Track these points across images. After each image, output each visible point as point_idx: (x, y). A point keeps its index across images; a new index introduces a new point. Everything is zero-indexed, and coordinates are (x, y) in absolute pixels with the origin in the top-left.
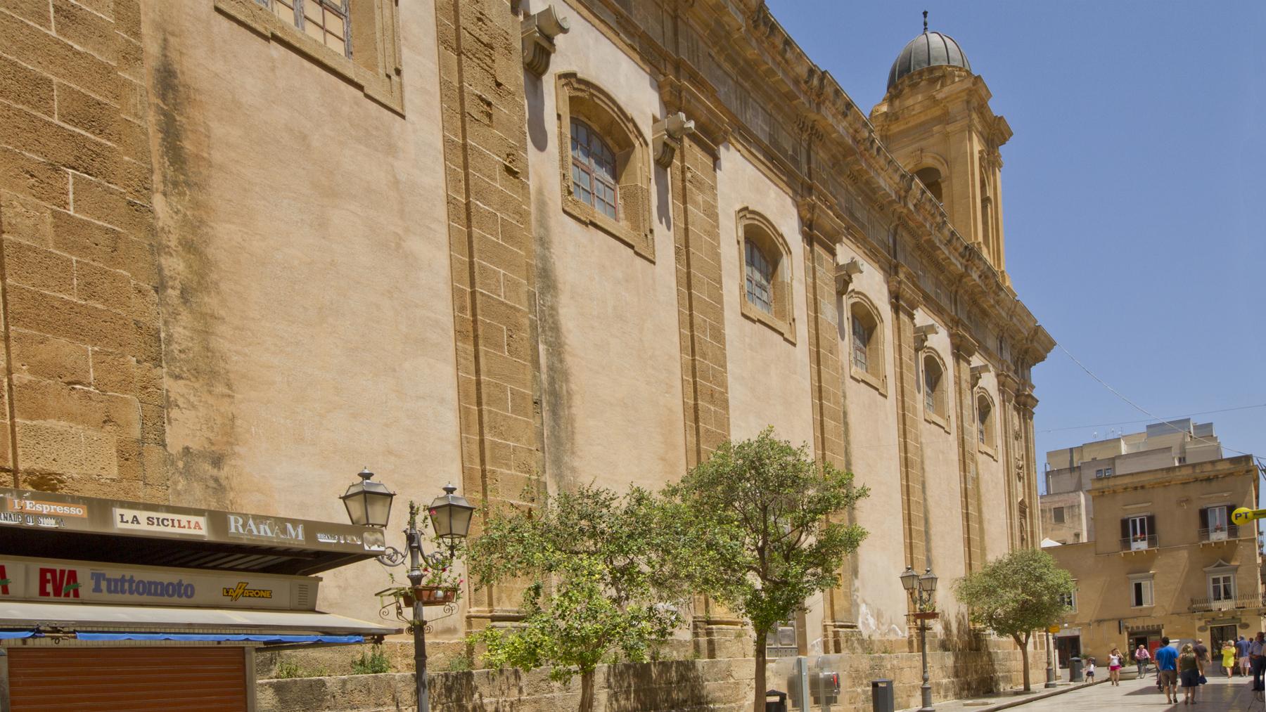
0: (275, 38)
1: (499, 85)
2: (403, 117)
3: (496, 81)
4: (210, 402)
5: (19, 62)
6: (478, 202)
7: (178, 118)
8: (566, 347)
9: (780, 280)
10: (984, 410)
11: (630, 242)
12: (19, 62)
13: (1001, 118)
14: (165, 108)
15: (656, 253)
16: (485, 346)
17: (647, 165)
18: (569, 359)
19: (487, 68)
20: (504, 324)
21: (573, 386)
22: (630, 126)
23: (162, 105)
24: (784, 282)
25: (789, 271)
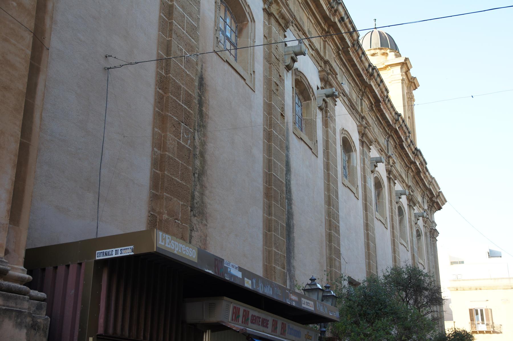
0: (227, 62)
1: (280, 76)
2: (254, 92)
3: (280, 75)
4: (201, 228)
5: (176, 80)
6: (274, 131)
7: (203, 98)
8: (293, 201)
9: (352, 165)
10: (419, 235)
11: (311, 147)
12: (176, 80)
13: (415, 77)
14: (200, 94)
15: (318, 152)
16: (274, 201)
17: (315, 109)
18: (293, 207)
19: (277, 69)
20: (279, 190)
21: (295, 222)
22: (311, 90)
23: (199, 93)
24: (353, 166)
25: (356, 160)
